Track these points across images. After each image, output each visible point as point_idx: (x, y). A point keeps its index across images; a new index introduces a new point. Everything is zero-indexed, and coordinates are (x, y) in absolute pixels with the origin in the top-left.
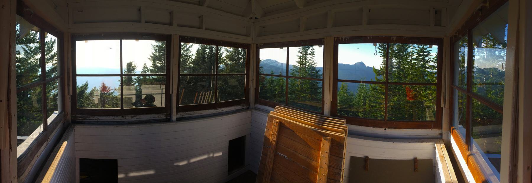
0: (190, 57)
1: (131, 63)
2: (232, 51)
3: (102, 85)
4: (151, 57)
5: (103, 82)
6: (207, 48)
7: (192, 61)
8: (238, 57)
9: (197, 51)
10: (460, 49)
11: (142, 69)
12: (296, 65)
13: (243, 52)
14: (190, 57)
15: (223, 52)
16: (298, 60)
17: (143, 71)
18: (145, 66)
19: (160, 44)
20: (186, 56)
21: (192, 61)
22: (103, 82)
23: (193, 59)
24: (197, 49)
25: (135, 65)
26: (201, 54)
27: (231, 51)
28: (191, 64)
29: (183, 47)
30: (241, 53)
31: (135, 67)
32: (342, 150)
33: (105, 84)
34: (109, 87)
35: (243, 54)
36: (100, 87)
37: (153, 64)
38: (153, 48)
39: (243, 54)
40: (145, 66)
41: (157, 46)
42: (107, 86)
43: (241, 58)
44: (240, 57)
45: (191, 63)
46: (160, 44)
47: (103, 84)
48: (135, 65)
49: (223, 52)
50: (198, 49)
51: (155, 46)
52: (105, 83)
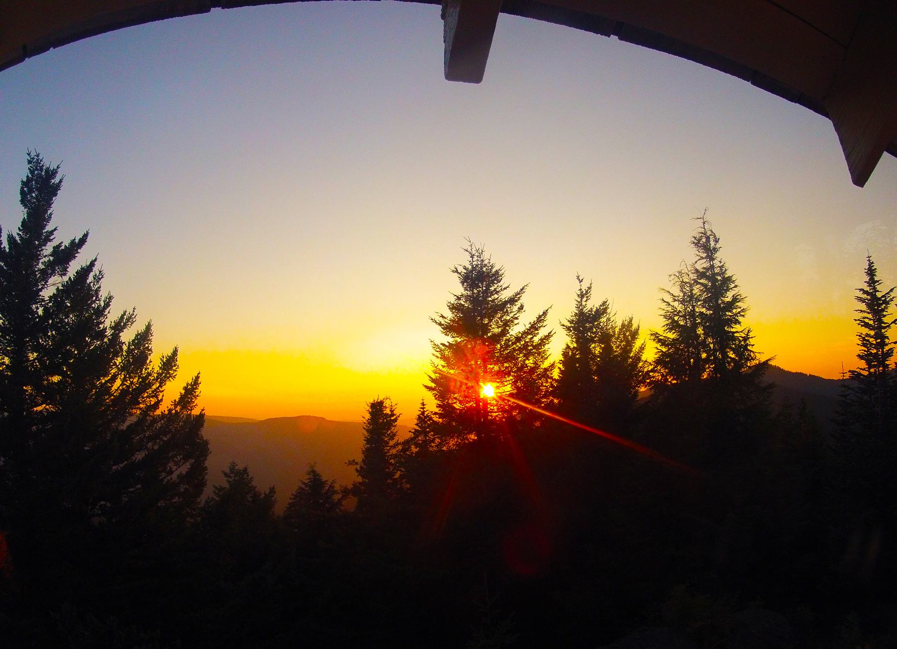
0: (546, 374)
1: (381, 403)
2: (677, 339)
3: (308, 477)
4: (433, 380)
5: (312, 467)
6: (595, 342)
7: (552, 386)
8: (698, 359)
9: (565, 354)
10: (176, 482)
11: (416, 421)
12: (858, 370)
13: (710, 340)
14: (546, 374)
15: (642, 348)
16: (860, 350)
17: (417, 428)
18: (423, 413)
19: (459, 340)
20: (533, 370)
21: (552, 386)
22: (312, 467)
23: (556, 381)
24: (564, 346)
25: (392, 411)
26: (578, 360)
27: (673, 340)
28: (551, 398)
29: (523, 343)
30: (704, 344)
31: (393, 415)
32: (497, 419)
33: (318, 475)
34: (329, 483)
35: (712, 346)
36: (304, 483)
37: (439, 406)
38: (438, 354)
39: (712, 346)
40: (423, 413)
41: (450, 346)
42: (324, 479)
43: (707, 360)
44: (704, 355)
45: (553, 393)
46: (459, 340)
47: (314, 472)
48: (392, 411)
49: (642, 348)
50: (568, 347)
51: (444, 345)
52: (318, 469)
